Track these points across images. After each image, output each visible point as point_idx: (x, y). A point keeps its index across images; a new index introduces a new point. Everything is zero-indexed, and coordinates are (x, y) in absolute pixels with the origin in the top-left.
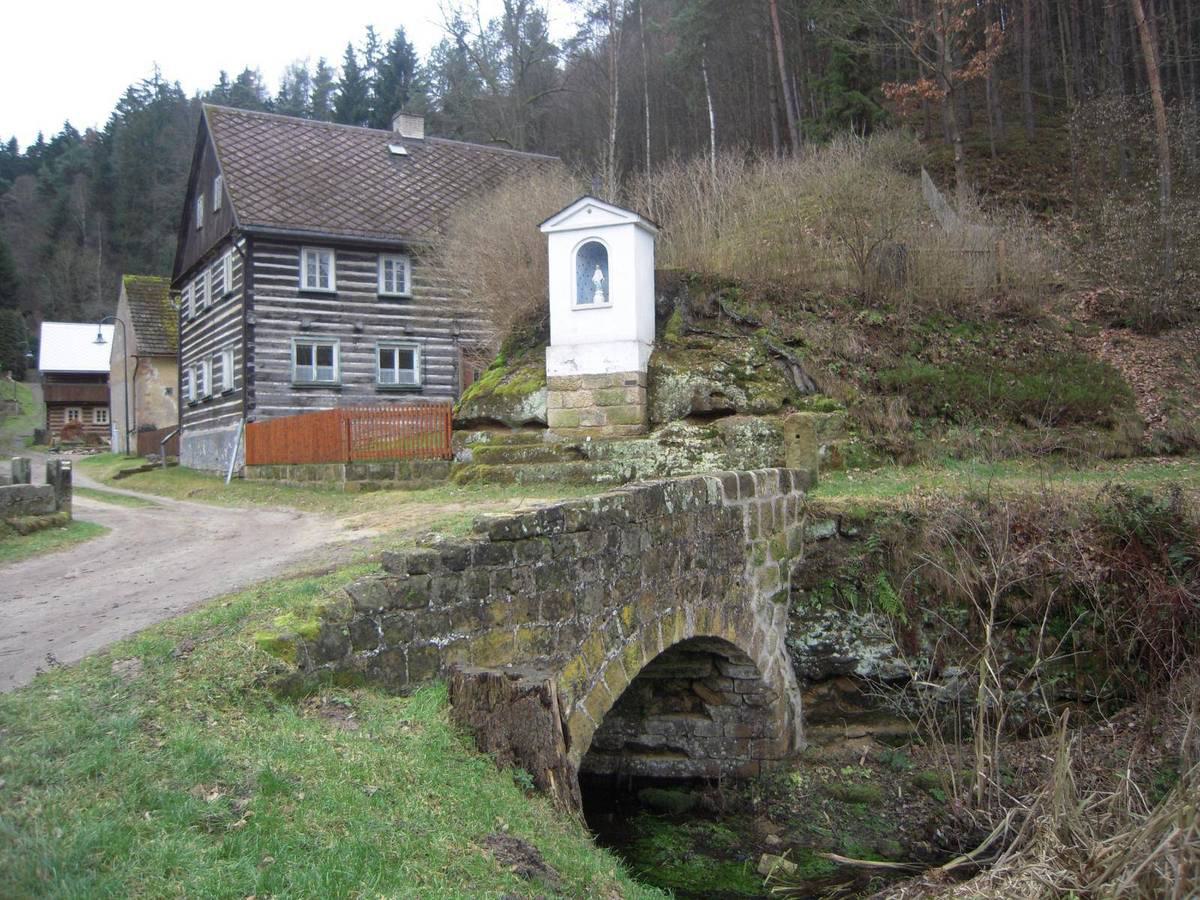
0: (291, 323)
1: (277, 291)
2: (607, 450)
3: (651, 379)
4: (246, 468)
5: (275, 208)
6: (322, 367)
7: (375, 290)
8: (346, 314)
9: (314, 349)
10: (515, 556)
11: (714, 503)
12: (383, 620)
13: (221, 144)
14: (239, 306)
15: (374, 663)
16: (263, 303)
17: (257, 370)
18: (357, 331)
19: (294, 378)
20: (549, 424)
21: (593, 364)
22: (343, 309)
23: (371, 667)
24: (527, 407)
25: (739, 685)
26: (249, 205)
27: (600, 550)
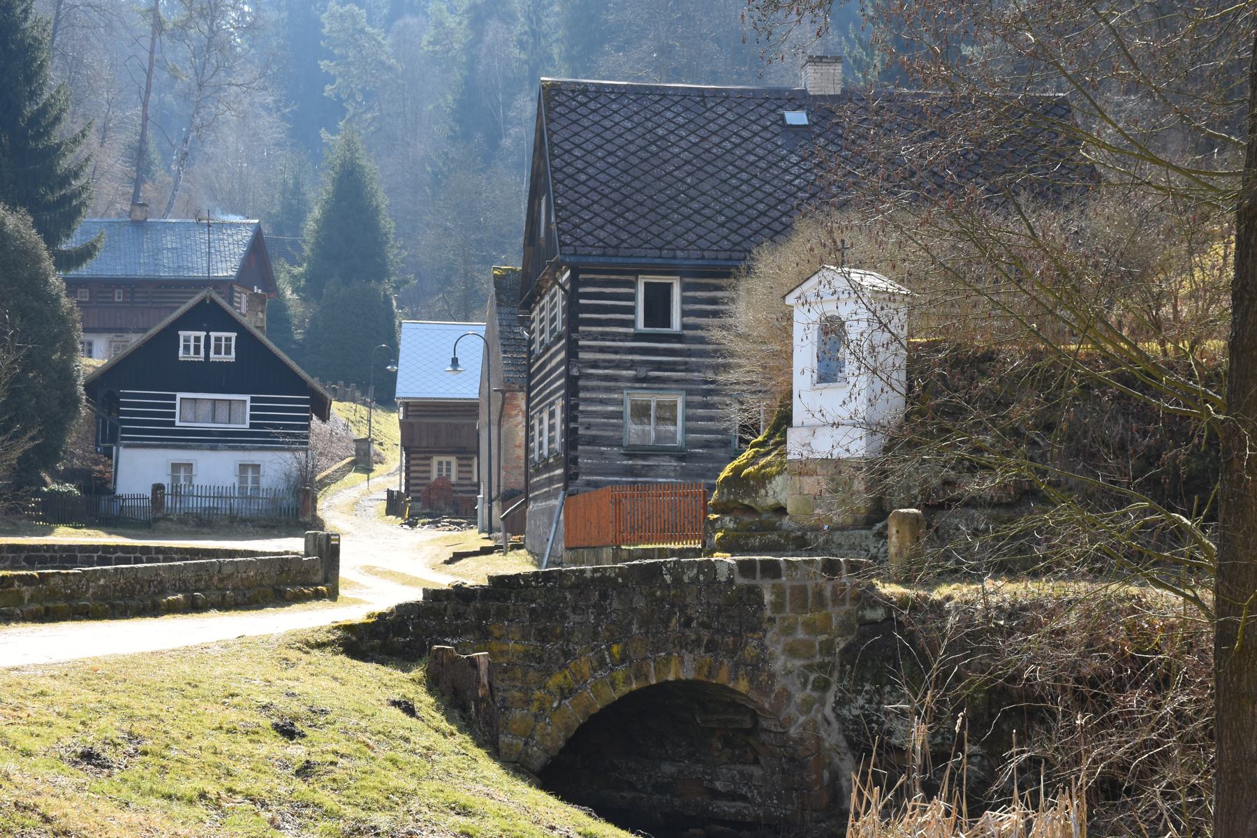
0: (624, 372)
1: (607, 334)
5: (609, 227)
9: (653, 405)
11: (723, 579)
13: (556, 139)
14: (562, 355)
15: (407, 645)
21: (825, 445)
22: (689, 353)
24: (771, 493)
26: (576, 226)
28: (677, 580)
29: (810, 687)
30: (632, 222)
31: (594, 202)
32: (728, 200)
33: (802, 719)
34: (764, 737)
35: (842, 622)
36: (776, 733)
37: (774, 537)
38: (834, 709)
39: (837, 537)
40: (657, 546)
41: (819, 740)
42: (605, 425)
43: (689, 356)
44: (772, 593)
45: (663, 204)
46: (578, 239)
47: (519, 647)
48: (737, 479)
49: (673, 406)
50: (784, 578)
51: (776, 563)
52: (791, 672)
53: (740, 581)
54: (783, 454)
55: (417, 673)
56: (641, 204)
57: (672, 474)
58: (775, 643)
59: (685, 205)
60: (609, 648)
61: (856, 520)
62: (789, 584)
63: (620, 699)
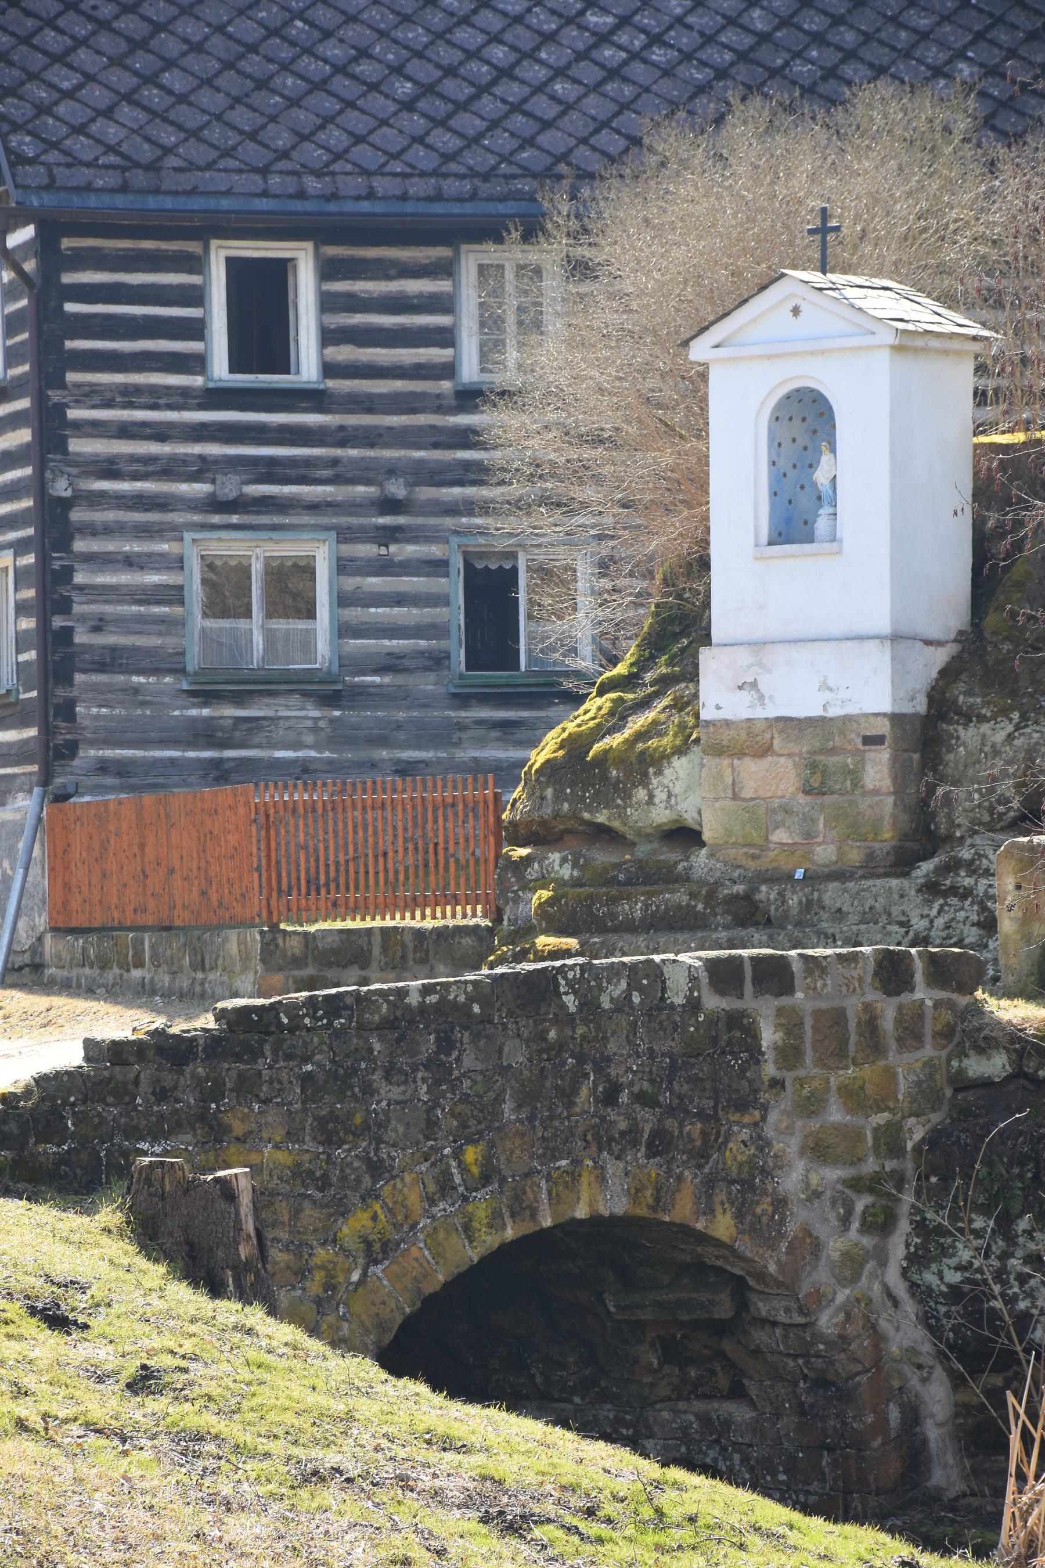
0: (184, 488)
1: (138, 389)
2: (809, 902)
3: (925, 735)
4: (48, 939)
5: (126, 112)
6: (280, 625)
7: (449, 370)
8: (353, 452)
9: (257, 568)
10: (268, 1053)
12: (74, 1113)
15: (63, 1159)
16: (96, 430)
17: (81, 637)
18: (390, 505)
19: (193, 662)
20: (707, 836)
22: (343, 437)
23: (57, 1165)
24: (660, 796)
25: (785, 1337)
26: (43, 109)
27: (423, 1057)
28: (589, 1004)
29: (856, 1225)
30: (182, 99)
31: (80, 42)
32: (416, 35)
33: (843, 1295)
34: (761, 1337)
35: (918, 1083)
36: (787, 1327)
37: (680, 897)
38: (904, 1273)
39: (831, 894)
40: (378, 923)
41: (878, 1338)
42: (139, 619)
43: (342, 444)
44: (778, 1026)
45: (253, 48)
46: (54, 145)
47: (283, 1158)
48: (576, 765)
49: (306, 570)
50: (799, 995)
51: (782, 963)
52: (817, 1195)
53: (713, 1002)
54: (687, 704)
55: (109, 1215)
56: (198, 48)
57: (309, 739)
58: (784, 1130)
59: (309, 51)
60: (458, 1154)
61: (870, 856)
62: (809, 1006)
63: (483, 1260)
